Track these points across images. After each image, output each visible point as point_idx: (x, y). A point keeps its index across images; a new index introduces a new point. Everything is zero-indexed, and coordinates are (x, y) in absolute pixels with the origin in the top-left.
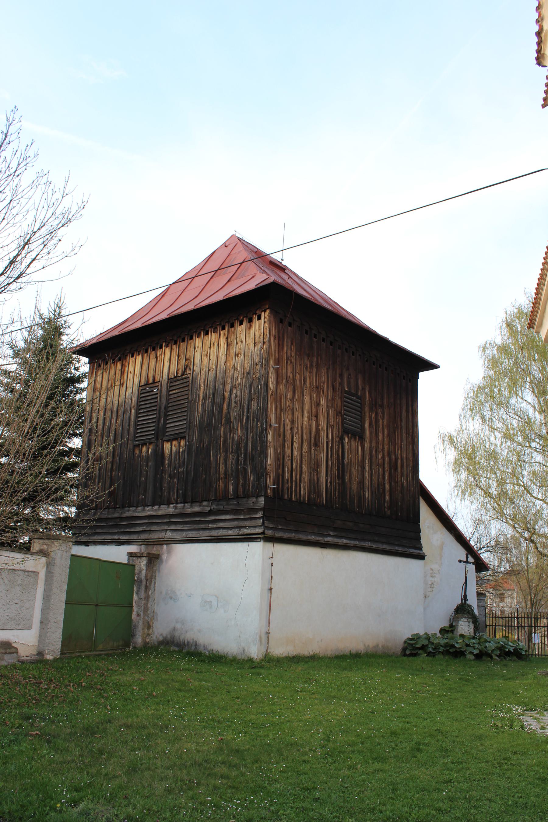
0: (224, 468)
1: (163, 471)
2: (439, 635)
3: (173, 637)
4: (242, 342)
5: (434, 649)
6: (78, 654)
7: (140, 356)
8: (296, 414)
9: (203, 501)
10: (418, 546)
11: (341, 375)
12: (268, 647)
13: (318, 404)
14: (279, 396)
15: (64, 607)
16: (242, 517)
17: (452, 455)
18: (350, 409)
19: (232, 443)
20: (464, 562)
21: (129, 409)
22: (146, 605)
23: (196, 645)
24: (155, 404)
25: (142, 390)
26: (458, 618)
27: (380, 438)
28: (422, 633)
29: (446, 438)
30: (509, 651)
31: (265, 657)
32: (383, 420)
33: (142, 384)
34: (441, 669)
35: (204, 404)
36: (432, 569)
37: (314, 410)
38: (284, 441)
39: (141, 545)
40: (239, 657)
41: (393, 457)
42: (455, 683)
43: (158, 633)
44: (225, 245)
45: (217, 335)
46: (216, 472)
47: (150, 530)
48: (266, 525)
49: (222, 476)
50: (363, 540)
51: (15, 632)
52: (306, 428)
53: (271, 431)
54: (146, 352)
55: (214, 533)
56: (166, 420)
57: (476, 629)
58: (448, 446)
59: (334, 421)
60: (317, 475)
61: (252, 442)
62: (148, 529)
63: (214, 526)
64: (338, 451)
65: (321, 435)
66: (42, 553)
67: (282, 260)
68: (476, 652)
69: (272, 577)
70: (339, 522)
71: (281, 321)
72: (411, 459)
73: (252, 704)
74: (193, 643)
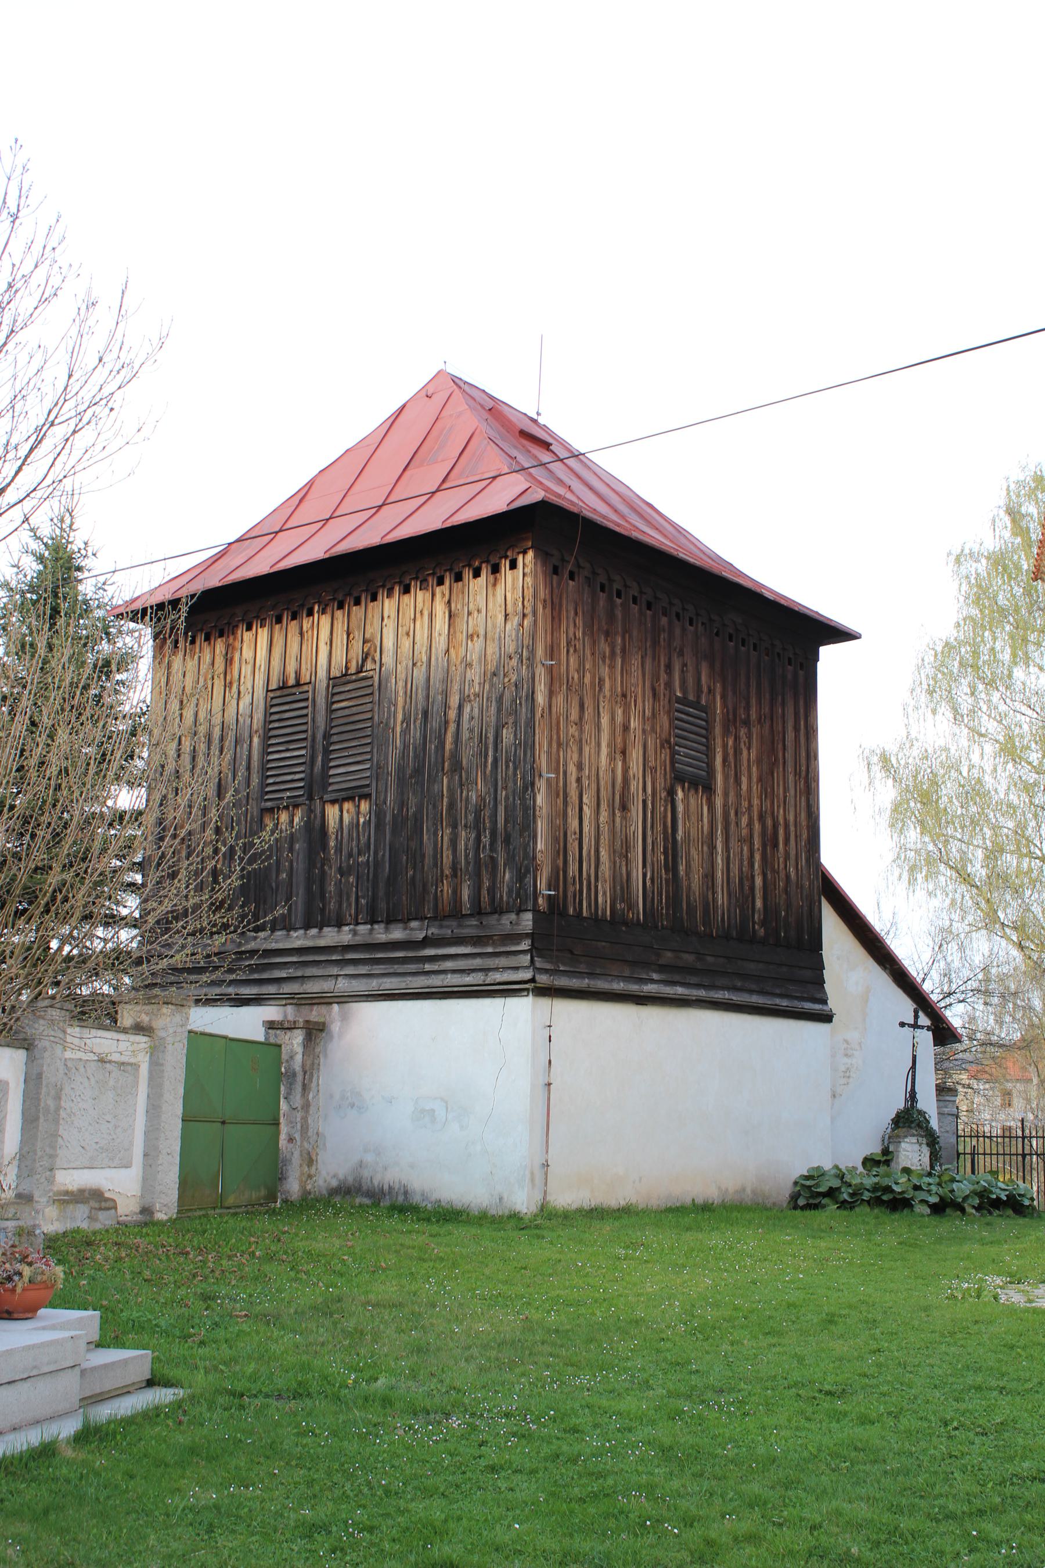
0: (451, 857)
1: (326, 861)
2: (861, 1169)
3: (359, 1181)
4: (479, 611)
5: (852, 1195)
6: (201, 1213)
7: (266, 629)
8: (586, 749)
9: (409, 920)
10: (818, 996)
11: (669, 667)
12: (545, 1192)
13: (626, 728)
14: (554, 716)
15: (180, 1126)
16: (490, 950)
17: (887, 793)
18: (686, 734)
19: (466, 808)
20: (910, 1025)
21: (247, 735)
22: (305, 1119)
23: (406, 1193)
24: (304, 728)
25: (272, 698)
26: (898, 1136)
27: (744, 787)
28: (827, 1166)
29: (875, 759)
30: (998, 1199)
31: (542, 1210)
32: (749, 749)
33: (273, 685)
34: (865, 1230)
35: (405, 732)
36: (846, 1041)
37: (619, 740)
38: (565, 803)
39: (285, 1005)
40: (493, 1212)
41: (769, 822)
42: (891, 1249)
43: (328, 1174)
44: (426, 394)
45: (428, 595)
46: (436, 865)
47: (303, 977)
48: (538, 965)
49: (447, 872)
50: (712, 987)
51: (108, 1173)
52: (605, 778)
53: (541, 785)
54: (279, 620)
55: (436, 981)
56: (326, 760)
57: (934, 1157)
58: (879, 775)
59: (656, 760)
60: (627, 865)
61: (506, 807)
62: (299, 974)
63: (435, 967)
64: (665, 817)
65: (633, 789)
66: (139, 1029)
67: (538, 414)
68: (934, 1200)
69: (550, 1062)
70: (669, 954)
71: (556, 571)
72: (804, 823)
73: (550, 1275)
74: (399, 1189)
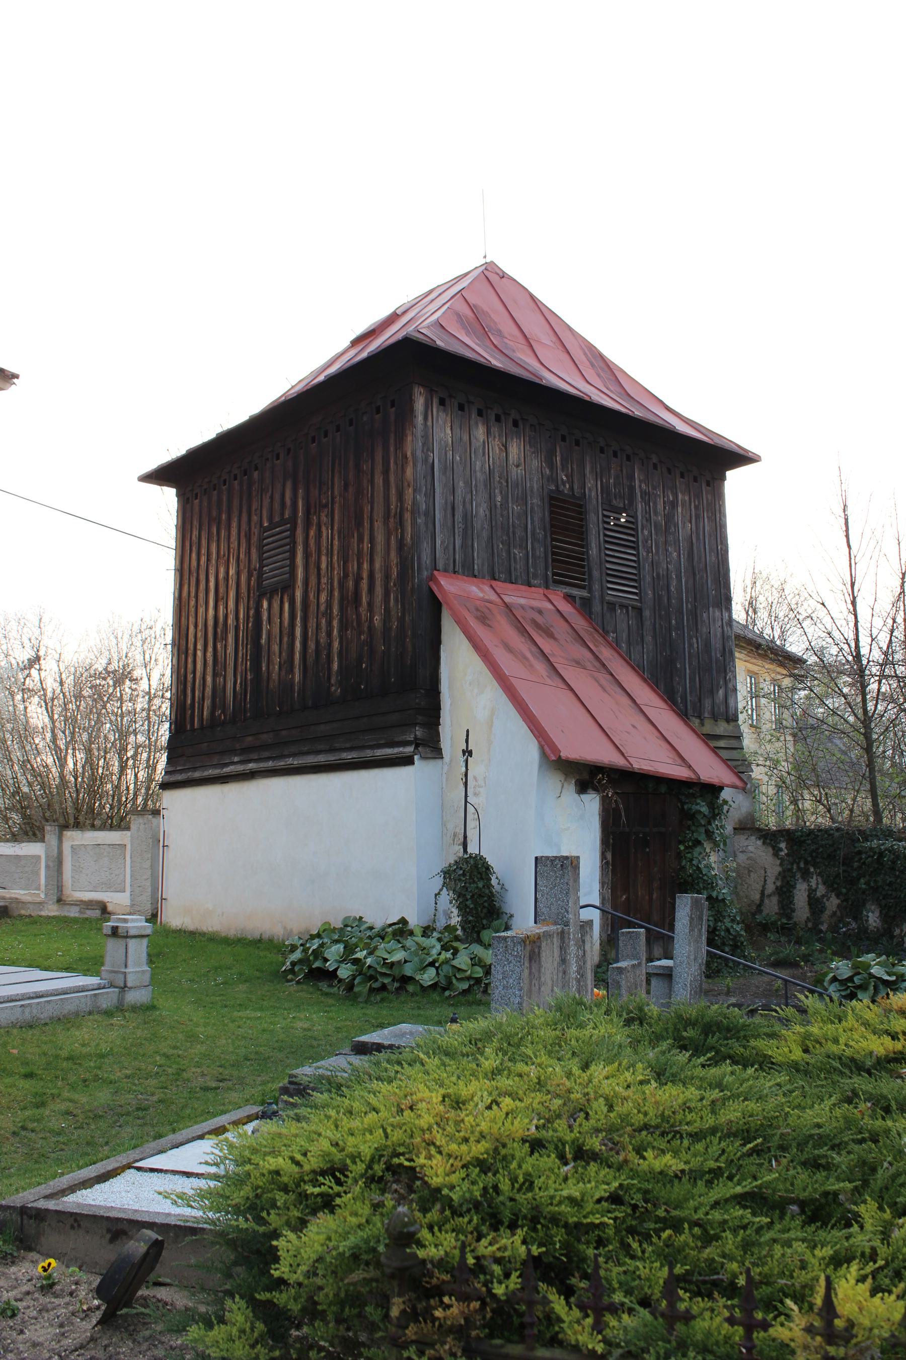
70: (250, 739)
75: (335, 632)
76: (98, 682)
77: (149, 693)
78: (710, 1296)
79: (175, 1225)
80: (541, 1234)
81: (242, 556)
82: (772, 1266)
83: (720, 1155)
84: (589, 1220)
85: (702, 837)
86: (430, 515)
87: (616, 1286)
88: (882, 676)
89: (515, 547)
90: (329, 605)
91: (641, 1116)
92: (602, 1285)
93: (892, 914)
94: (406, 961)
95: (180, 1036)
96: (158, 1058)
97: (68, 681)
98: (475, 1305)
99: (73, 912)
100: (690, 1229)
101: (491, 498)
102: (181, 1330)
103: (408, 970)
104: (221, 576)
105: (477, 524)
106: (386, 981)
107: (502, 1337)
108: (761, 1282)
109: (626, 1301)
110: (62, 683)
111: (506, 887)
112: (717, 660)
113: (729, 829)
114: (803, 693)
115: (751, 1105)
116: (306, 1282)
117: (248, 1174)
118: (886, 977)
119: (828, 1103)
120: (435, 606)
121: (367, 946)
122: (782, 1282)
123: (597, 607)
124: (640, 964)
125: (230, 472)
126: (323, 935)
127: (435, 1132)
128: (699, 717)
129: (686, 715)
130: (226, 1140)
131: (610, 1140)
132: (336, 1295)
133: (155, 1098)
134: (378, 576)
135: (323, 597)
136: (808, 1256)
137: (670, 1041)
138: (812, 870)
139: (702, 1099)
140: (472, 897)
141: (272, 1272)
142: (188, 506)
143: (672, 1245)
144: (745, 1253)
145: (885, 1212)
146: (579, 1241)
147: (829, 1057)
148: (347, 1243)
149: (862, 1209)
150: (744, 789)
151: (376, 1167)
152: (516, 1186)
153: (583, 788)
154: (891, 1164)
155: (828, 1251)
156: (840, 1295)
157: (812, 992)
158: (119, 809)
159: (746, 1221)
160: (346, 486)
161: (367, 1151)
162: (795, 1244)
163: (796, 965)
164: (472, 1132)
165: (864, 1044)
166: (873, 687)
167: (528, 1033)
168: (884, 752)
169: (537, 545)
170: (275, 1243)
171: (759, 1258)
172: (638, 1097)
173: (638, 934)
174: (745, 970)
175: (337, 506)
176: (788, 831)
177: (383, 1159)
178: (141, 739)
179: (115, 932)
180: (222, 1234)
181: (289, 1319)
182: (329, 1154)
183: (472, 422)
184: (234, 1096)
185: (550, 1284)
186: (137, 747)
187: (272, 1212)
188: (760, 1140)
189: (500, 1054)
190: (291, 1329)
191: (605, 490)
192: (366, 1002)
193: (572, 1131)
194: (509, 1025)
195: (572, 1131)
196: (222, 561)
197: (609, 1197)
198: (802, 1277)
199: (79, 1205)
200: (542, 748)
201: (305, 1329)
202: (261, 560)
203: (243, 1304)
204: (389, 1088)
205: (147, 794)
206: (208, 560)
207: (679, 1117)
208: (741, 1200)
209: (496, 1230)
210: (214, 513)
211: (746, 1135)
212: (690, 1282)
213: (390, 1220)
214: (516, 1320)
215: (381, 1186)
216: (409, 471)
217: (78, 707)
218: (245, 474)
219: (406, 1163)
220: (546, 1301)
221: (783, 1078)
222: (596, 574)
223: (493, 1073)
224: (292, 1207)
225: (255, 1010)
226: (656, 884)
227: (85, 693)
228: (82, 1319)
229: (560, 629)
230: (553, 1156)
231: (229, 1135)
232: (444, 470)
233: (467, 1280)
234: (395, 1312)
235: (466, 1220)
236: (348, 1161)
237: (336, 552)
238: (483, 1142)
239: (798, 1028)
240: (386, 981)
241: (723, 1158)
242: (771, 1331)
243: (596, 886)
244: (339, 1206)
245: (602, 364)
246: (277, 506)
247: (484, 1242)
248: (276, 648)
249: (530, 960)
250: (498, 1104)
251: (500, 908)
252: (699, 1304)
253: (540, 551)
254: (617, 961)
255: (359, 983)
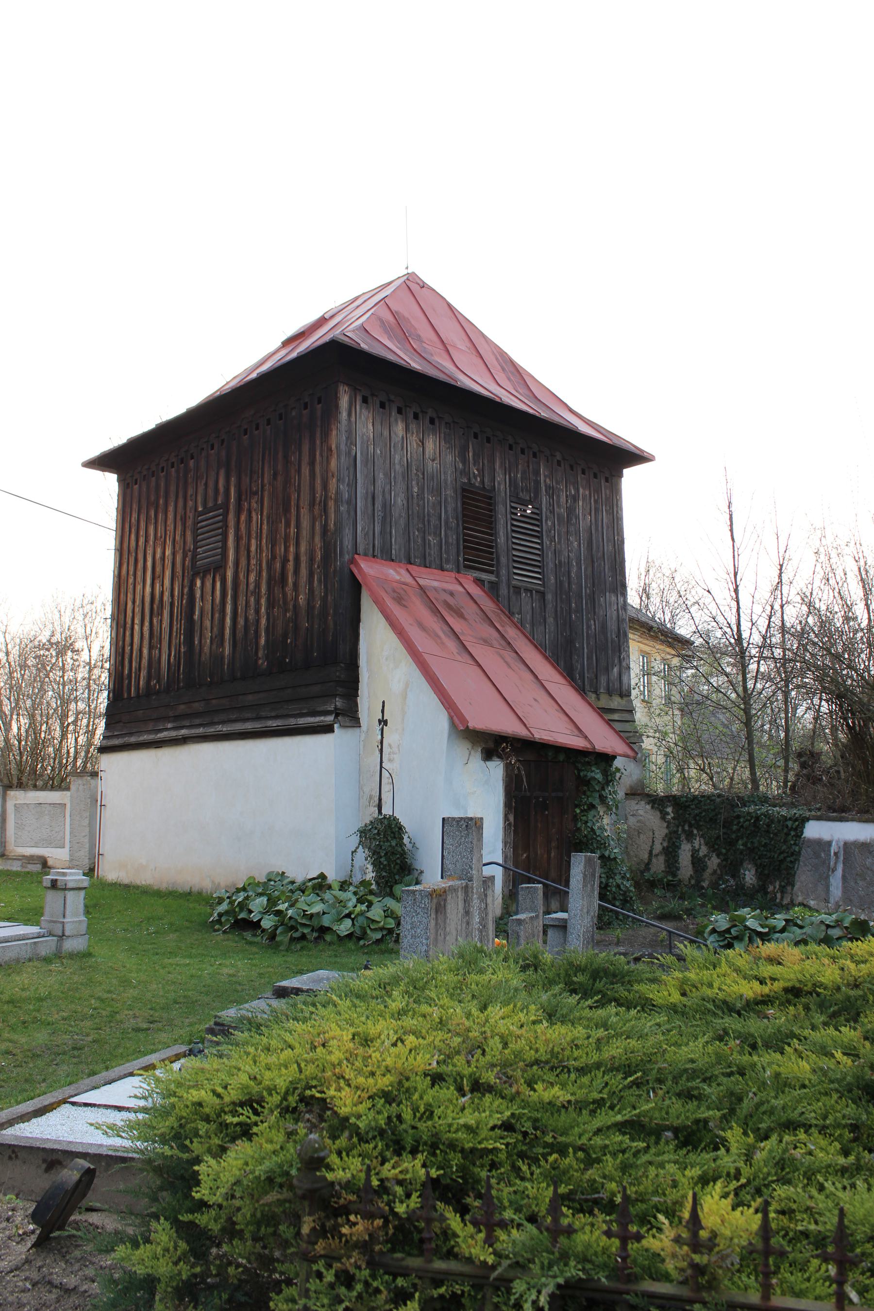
50: (212, 724)
70: (182, 707)
75: (263, 610)
76: (42, 652)
77: (89, 664)
78: (591, 1213)
79: (107, 1155)
80: (440, 1158)
81: (178, 538)
82: (647, 1185)
83: (604, 1088)
84: (483, 1146)
85: (596, 802)
86: (352, 503)
87: (507, 1204)
88: (761, 657)
89: (429, 534)
90: (258, 585)
91: (532, 1052)
92: (493, 1204)
93: (766, 872)
94: (324, 913)
95: (114, 981)
96: (93, 1001)
97: (14, 651)
98: (379, 1222)
99: (16, 867)
100: (575, 1153)
101: (408, 489)
102: (110, 1250)
103: (326, 921)
104: (158, 556)
105: (396, 513)
106: (306, 931)
107: (403, 1251)
108: (637, 1200)
109: (516, 1217)
110: (7, 654)
111: (417, 845)
112: (613, 641)
113: (621, 795)
114: (690, 672)
115: (633, 1043)
116: (225, 1203)
117: (173, 1106)
118: (760, 929)
119: (702, 1040)
120: (355, 587)
121: (288, 899)
122: (656, 1199)
123: (504, 591)
124: (537, 916)
125: (168, 460)
126: (248, 888)
127: (344, 1066)
128: (596, 692)
129: (584, 690)
130: (154, 1076)
131: (505, 1074)
132: (253, 1215)
133: (90, 1039)
134: (304, 559)
135: (252, 578)
136: (679, 1177)
137: (561, 986)
138: (695, 832)
139: (588, 1037)
140: (386, 854)
141: (193, 1194)
142: (129, 491)
143: (558, 1167)
144: (624, 1174)
145: (748, 1136)
146: (474, 1164)
147: (704, 1000)
148: (263, 1167)
149: (728, 1134)
150: (635, 758)
151: (290, 1098)
152: (418, 1115)
153: (488, 755)
154: (755, 1094)
155: (696, 1172)
156: (706, 1210)
157: (692, 942)
158: (60, 771)
159: (624, 1146)
160: (275, 476)
161: (282, 1084)
162: (667, 1166)
163: (679, 918)
164: (379, 1067)
165: (735, 988)
166: (753, 667)
167: (433, 978)
168: (763, 726)
169: (449, 533)
170: (196, 1168)
171: (636, 1179)
172: (531, 1035)
173: (536, 889)
174: (633, 923)
175: (266, 494)
176: (674, 797)
177: (297, 1092)
178: (81, 706)
179: (54, 884)
180: (150, 1161)
181: (210, 1238)
182: (247, 1087)
183: (392, 419)
184: (163, 1036)
185: (447, 1202)
186: (78, 713)
187: (195, 1140)
188: (639, 1074)
189: (406, 997)
190: (211, 1247)
191: (513, 483)
192: (287, 951)
193: (469, 1066)
194: (415, 970)
195: (469, 1066)
196: (159, 542)
197: (502, 1125)
198: (673, 1195)
199: (16, 1137)
200: (451, 718)
201: (225, 1248)
202: (195, 542)
203: (167, 1225)
204: (304, 1027)
205: (86, 756)
206: (146, 541)
207: (567, 1053)
208: (621, 1127)
209: (399, 1155)
210: (153, 498)
211: (627, 1069)
212: (574, 1200)
213: (302, 1146)
214: (416, 1236)
215: (296, 1116)
216: (333, 463)
217: (23, 676)
218: (182, 462)
219: (318, 1095)
220: (443, 1218)
221: (662, 1018)
222: (503, 560)
223: (399, 1013)
224: (213, 1136)
225: (184, 957)
226: (554, 844)
227: (29, 663)
228: (18, 1243)
229: (470, 610)
230: (452, 1088)
231: (158, 1072)
232: (366, 463)
233: (371, 1201)
234: (305, 1230)
235: (372, 1146)
236: (265, 1093)
237: (264, 536)
238: (388, 1076)
239: (677, 974)
240: (306, 931)
241: (606, 1090)
242: (644, 1242)
243: (500, 845)
244: (257, 1134)
245: (512, 369)
246: (211, 492)
247: (387, 1166)
248: (208, 623)
249: (437, 912)
250: (402, 1042)
251: (411, 864)
252: (582, 1219)
253: (452, 539)
254: (517, 913)
255: (281, 933)
